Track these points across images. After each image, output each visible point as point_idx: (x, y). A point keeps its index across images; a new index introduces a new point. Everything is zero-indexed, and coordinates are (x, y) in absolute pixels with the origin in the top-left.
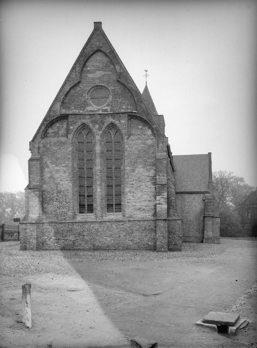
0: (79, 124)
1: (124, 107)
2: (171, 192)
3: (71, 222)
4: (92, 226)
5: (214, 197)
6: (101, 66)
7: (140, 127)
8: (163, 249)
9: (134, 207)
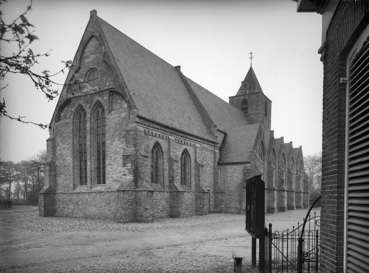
0: (77, 105)
1: (107, 84)
2: (139, 163)
3: (71, 193)
4: (84, 196)
5: (257, 167)
6: (94, 50)
7: (119, 101)
8: (122, 220)
9: (112, 178)
